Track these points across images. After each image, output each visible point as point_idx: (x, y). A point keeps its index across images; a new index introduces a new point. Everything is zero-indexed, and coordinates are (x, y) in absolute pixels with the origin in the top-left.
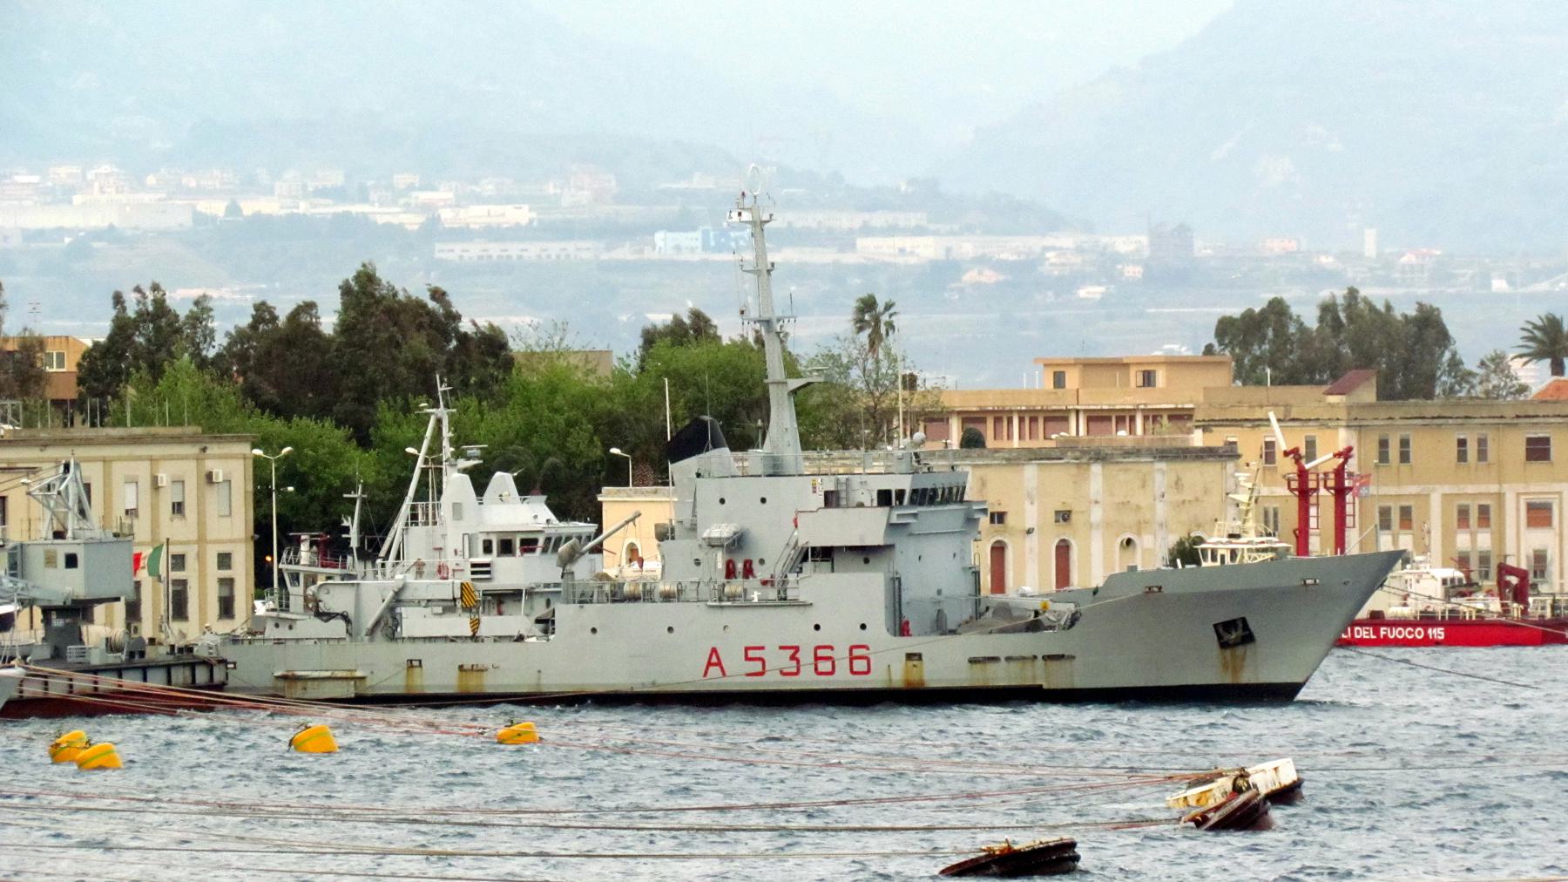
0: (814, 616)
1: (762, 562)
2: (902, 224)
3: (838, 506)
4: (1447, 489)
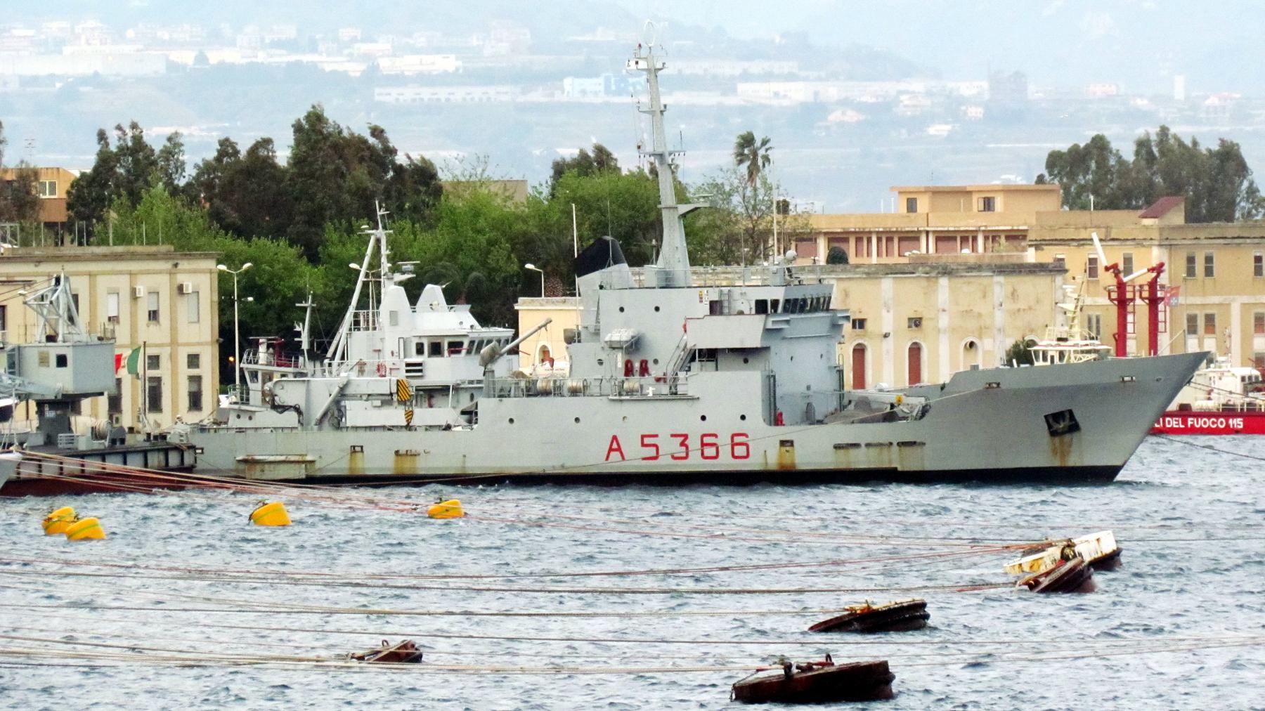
1: (656, 361)
3: (721, 313)
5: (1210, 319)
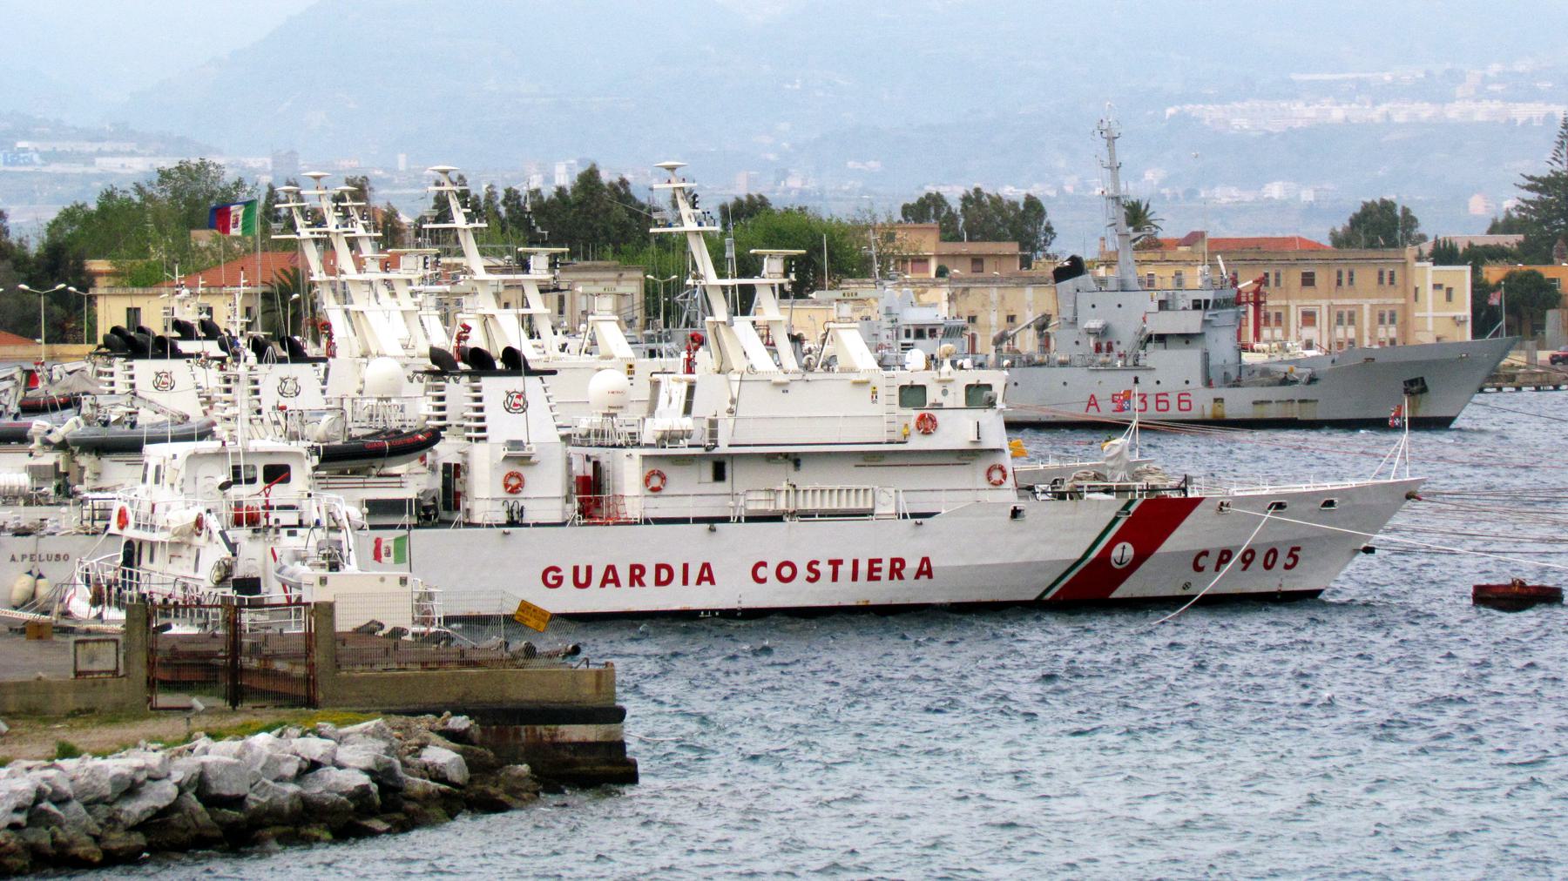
0: (1157, 375)
1: (1118, 343)
2: (122, 149)
3: (1167, 309)
4: (1375, 301)
5: (1351, 315)
